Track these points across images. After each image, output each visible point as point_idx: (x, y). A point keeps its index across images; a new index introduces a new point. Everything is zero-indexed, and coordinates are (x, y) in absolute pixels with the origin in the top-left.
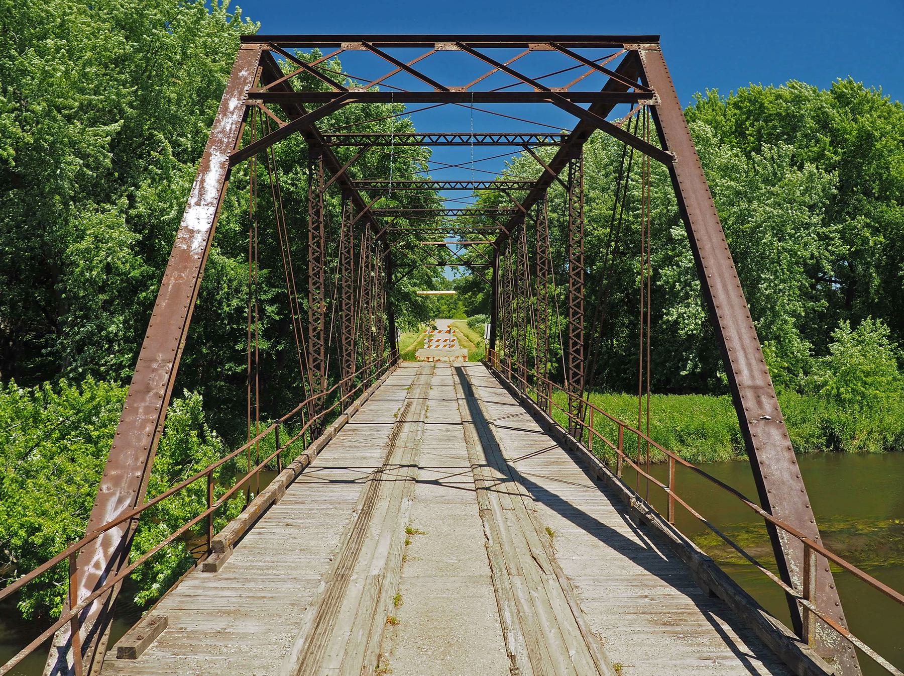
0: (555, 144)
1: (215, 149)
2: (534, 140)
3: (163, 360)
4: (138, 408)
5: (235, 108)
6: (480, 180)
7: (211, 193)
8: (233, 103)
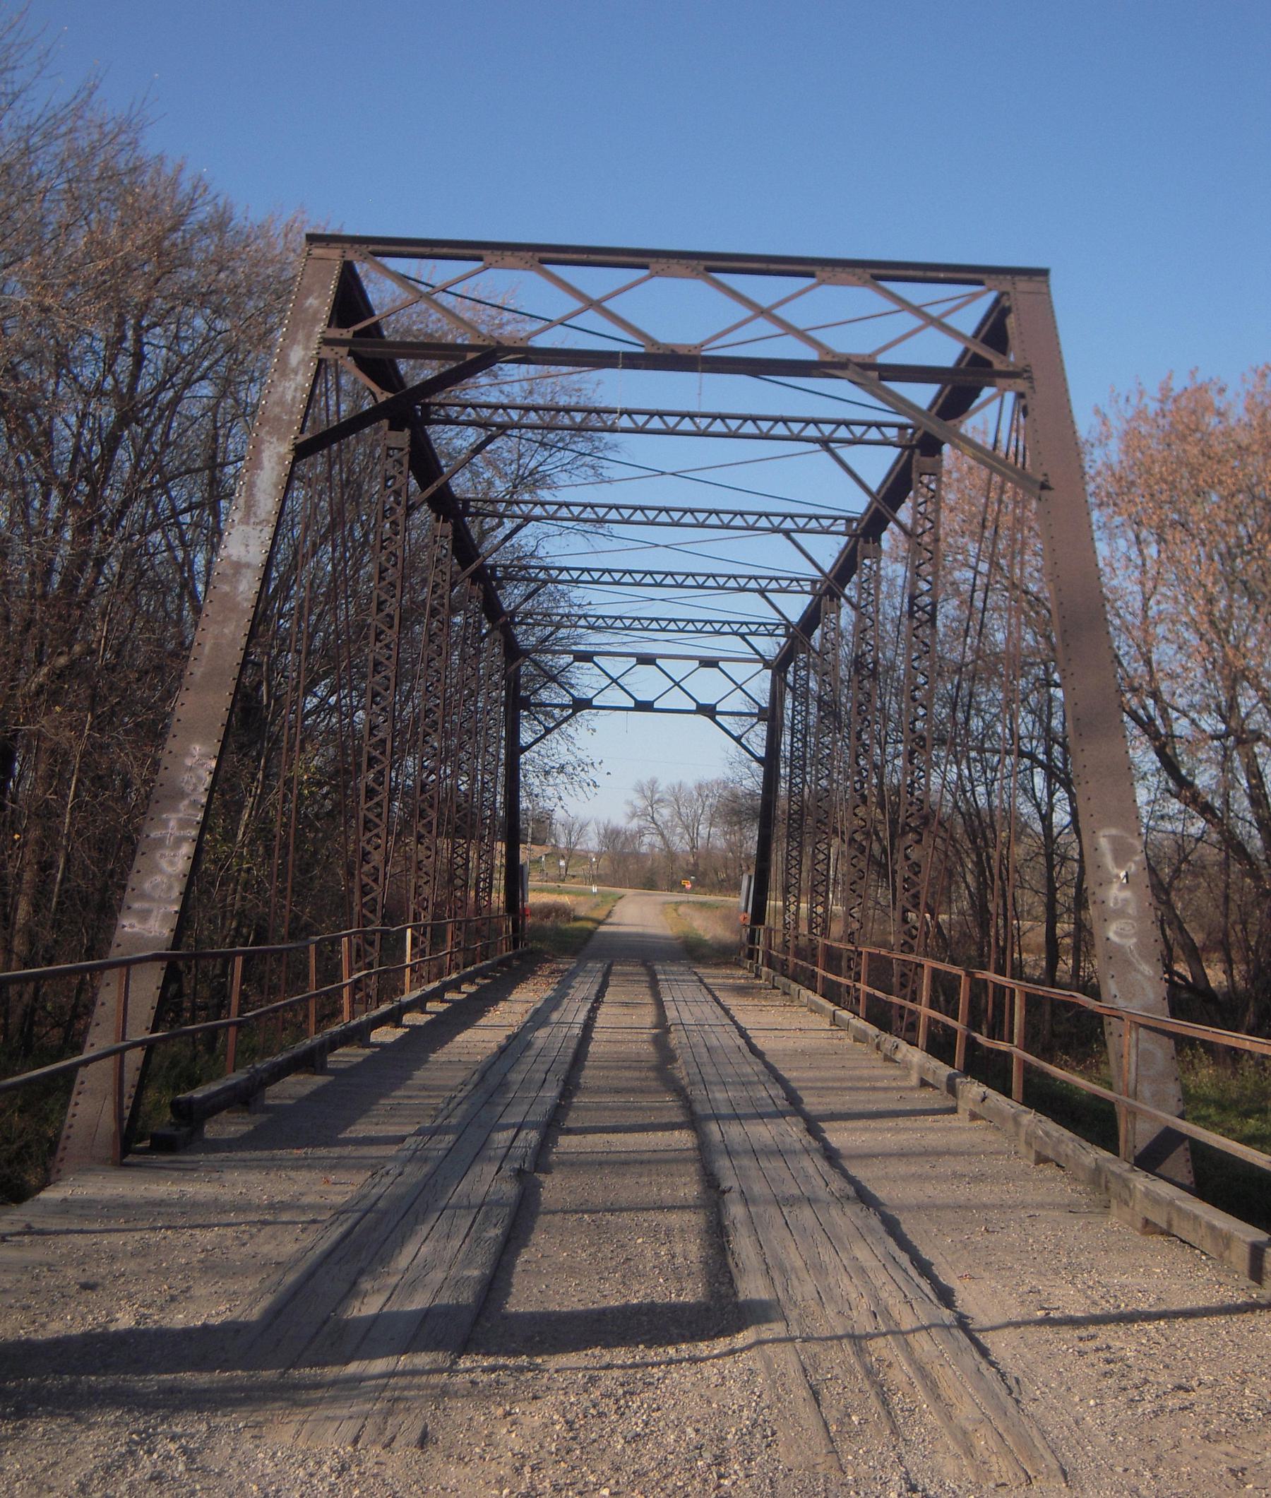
0: (885, 442)
1: (268, 433)
2: (843, 433)
3: (202, 755)
4: (168, 820)
5: (299, 363)
6: (736, 508)
7: (267, 503)
8: (297, 355)
